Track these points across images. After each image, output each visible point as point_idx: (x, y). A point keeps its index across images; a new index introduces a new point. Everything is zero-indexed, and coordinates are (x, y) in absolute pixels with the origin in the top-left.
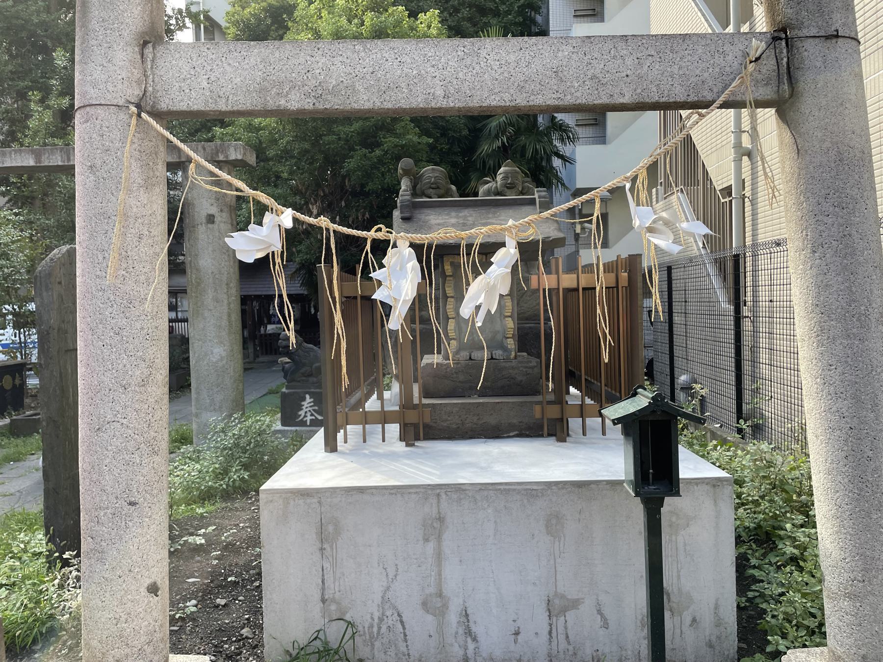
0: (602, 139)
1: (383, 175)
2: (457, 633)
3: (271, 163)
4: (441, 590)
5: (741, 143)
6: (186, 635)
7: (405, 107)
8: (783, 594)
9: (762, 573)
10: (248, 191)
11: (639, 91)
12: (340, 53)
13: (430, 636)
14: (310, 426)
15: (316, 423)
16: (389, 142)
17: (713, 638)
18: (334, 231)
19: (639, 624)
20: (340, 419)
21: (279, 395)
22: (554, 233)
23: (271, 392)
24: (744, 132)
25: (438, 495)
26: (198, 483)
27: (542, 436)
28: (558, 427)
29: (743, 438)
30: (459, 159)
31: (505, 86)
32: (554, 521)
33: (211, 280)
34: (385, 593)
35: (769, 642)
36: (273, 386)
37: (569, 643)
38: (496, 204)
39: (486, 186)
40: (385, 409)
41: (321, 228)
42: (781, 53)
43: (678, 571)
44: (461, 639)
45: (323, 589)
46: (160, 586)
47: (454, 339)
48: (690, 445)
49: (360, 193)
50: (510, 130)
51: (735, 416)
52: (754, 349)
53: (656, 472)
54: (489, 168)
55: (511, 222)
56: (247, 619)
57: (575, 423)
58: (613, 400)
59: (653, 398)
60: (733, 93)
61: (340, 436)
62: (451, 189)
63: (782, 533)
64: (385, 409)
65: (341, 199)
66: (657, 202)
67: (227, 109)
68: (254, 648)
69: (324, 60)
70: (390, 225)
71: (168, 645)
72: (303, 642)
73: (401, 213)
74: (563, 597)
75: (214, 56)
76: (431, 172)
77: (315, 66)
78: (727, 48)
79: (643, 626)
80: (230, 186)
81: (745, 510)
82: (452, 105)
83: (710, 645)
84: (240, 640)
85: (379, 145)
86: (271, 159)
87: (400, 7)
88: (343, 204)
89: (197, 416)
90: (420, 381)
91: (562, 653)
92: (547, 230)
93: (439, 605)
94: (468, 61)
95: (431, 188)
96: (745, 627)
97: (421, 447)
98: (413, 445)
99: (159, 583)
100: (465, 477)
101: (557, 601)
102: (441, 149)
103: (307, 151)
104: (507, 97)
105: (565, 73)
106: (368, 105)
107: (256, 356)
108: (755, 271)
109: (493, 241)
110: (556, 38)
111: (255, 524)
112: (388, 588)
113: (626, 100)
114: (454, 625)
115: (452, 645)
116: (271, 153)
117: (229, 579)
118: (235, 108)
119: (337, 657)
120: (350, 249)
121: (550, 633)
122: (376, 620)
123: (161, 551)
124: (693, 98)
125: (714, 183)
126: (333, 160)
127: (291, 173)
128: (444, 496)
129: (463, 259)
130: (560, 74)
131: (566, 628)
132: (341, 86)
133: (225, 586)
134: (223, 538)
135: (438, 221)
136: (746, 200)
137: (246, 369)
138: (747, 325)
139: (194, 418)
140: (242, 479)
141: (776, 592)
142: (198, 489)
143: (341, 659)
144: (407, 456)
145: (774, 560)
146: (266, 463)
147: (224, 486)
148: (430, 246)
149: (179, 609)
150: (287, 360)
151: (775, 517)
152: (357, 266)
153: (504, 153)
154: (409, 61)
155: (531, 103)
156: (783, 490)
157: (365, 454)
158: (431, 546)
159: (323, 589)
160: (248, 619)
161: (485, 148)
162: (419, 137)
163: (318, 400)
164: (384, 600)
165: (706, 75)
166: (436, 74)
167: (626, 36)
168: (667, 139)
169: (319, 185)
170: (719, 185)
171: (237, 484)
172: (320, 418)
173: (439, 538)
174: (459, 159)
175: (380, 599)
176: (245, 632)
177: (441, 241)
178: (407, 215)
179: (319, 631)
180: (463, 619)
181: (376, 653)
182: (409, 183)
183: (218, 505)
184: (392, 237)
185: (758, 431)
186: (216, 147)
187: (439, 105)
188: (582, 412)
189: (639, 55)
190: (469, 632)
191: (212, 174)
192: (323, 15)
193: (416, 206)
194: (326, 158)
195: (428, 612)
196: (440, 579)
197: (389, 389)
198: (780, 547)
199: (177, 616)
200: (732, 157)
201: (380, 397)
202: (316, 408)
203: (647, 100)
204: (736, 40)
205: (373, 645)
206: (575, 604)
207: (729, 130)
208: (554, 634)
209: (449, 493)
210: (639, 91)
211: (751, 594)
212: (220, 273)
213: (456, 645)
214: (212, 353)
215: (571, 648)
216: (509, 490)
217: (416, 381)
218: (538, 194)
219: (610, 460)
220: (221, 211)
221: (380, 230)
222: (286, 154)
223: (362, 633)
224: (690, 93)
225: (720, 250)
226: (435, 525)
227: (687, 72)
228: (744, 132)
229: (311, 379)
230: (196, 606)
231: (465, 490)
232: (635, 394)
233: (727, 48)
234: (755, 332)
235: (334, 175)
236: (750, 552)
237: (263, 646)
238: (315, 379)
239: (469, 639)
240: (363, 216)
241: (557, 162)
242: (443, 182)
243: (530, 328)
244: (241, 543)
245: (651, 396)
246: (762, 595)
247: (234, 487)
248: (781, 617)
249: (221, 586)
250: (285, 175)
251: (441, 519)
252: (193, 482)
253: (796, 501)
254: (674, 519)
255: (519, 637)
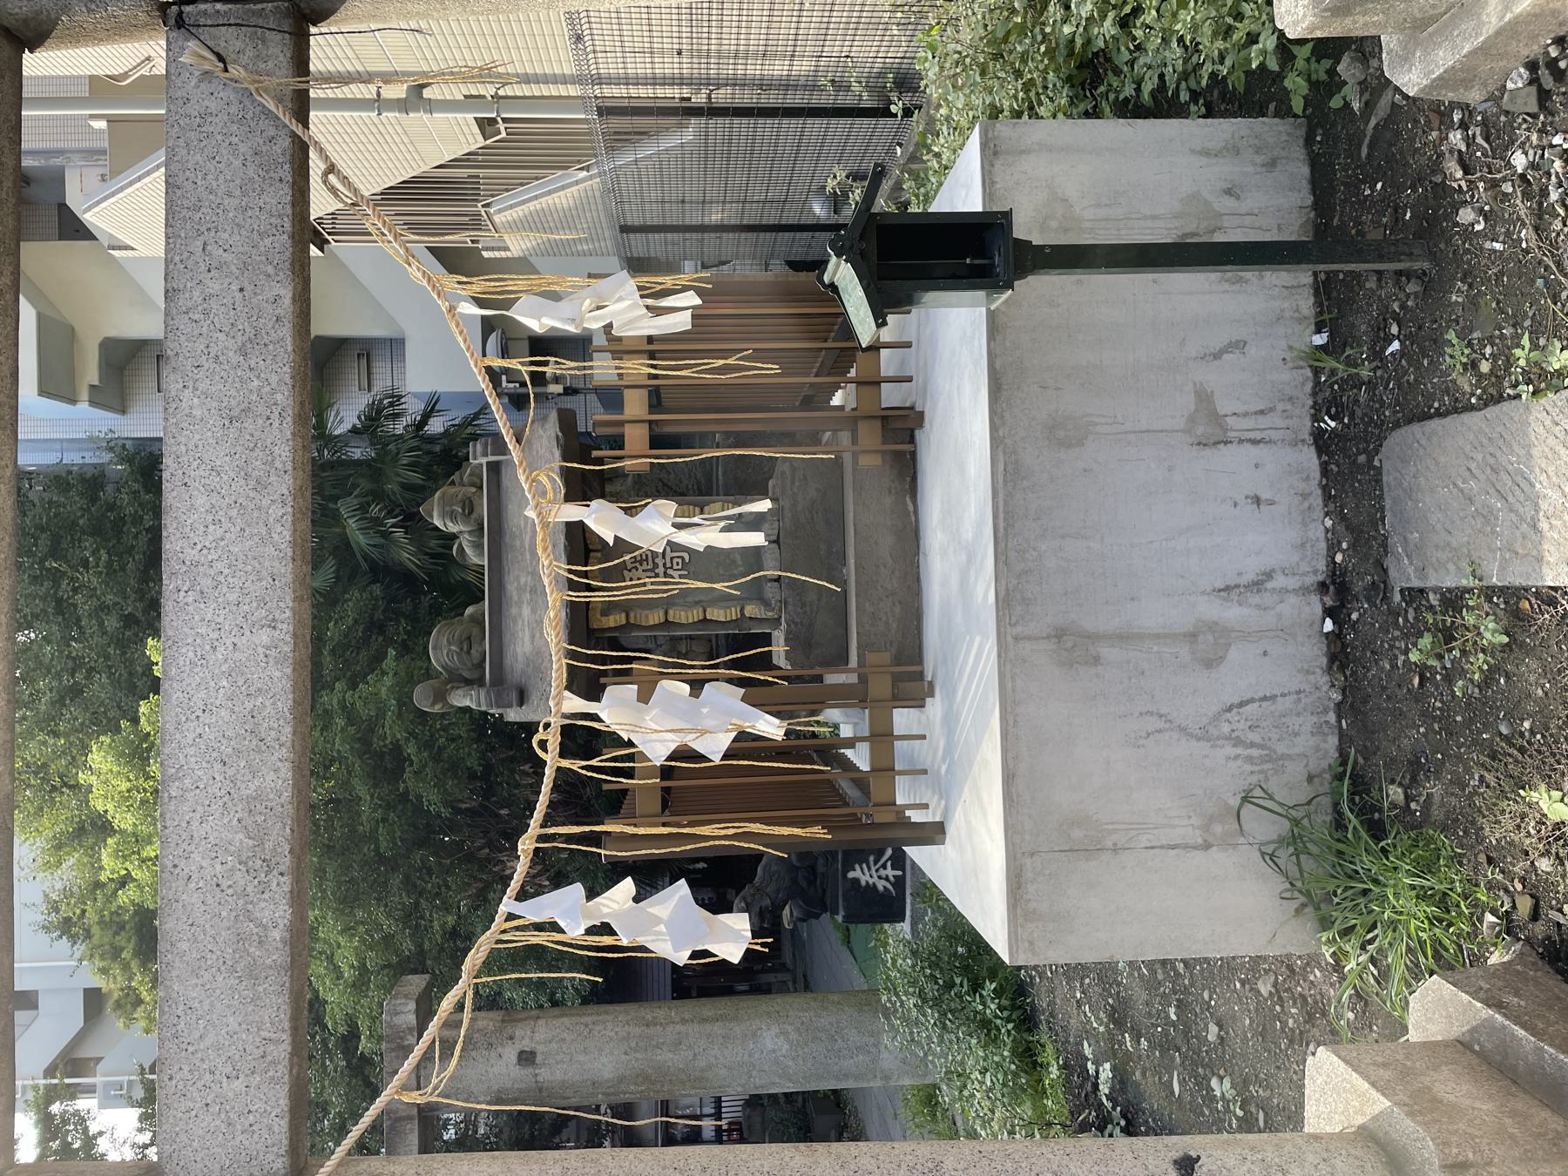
0: (395, 346)
1: (453, 740)
2: (1258, 607)
3: (427, 945)
4: (1185, 635)
5: (398, 100)
6: (1272, 1096)
7: (290, 702)
8: (1181, 40)
9: (1147, 78)
10: (463, 987)
11: (270, 269)
12: (184, 824)
13: (1265, 653)
14: (904, 870)
15: (899, 860)
16: (392, 730)
17: (1259, 159)
18: (542, 826)
19: (1236, 287)
20: (882, 817)
21: (852, 927)
22: (552, 428)
23: (847, 941)
24: (379, 94)
25: (1016, 639)
26: (1005, 1074)
27: (913, 454)
28: (898, 425)
29: (920, 108)
30: (426, 601)
31: (256, 514)
32: (1061, 434)
33: (638, 1055)
34: (1191, 735)
35: (1262, 66)
36: (837, 937)
37: (1271, 410)
38: (497, 534)
39: (468, 551)
40: (867, 734)
41: (537, 850)
42: (205, 12)
43: (1145, 218)
44: (1268, 600)
45: (1186, 847)
46: (1180, 1154)
47: (742, 610)
48: (928, 199)
49: (485, 780)
50: (375, 510)
51: (882, 121)
52: (763, 84)
53: (973, 252)
54: (443, 547)
55: (530, 513)
56: (1243, 985)
57: (891, 396)
58: (848, 332)
59: (838, 255)
60: (279, 100)
61: (916, 816)
62: (471, 616)
63: (1079, 41)
64: (867, 734)
65: (497, 816)
66: (506, 249)
67: (289, 1040)
68: (1293, 971)
69: (196, 857)
70: (530, 728)
71: (1288, 1135)
72: (1280, 884)
73: (511, 706)
74: (1192, 419)
75: (186, 1068)
76: (441, 649)
77: (208, 873)
78: (193, 109)
79: (1240, 280)
80: (452, 1024)
81: (1040, 103)
82: (288, 613)
83: (1272, 164)
84: (1280, 998)
85: (397, 748)
86: (420, 946)
87: (142, 710)
88: (504, 812)
89: (886, 1078)
90: (817, 671)
91: (1290, 422)
92: (545, 442)
93: (1210, 637)
94: (206, 583)
95: (469, 653)
96: (1240, 106)
97: (935, 668)
98: (931, 684)
99: (1177, 1155)
100: (984, 591)
101: (1200, 430)
102: (407, 633)
103: (407, 880)
104: (276, 511)
105: (233, 403)
106: (286, 771)
107: (783, 968)
108: (627, 81)
109: (562, 538)
110: (166, 419)
111: (1075, 972)
112: (1182, 729)
113: (286, 293)
114: (1245, 611)
115: (1280, 616)
116: (408, 946)
117: (1174, 1017)
118: (287, 1025)
119: (1305, 822)
120: (576, 799)
121: (1255, 442)
122: (1239, 751)
123: (1118, 1151)
124: (286, 172)
125: (473, 148)
126: (424, 831)
127: (446, 908)
128: (1019, 629)
129: (598, 598)
130: (235, 413)
131: (1246, 414)
132: (249, 821)
133: (1185, 1025)
134: (1102, 1029)
135: (527, 639)
136: (501, 93)
137: (807, 988)
138: (722, 96)
139: (892, 1083)
140: (998, 993)
141: (1179, 51)
142: (1015, 1075)
143: (1308, 816)
144: (950, 695)
145: (1126, 56)
146: (969, 951)
147: (1010, 1026)
148: (572, 655)
149: (1227, 1110)
150: (786, 911)
151: (1051, 53)
152: (606, 787)
153: (413, 521)
154: (202, 694)
155: (289, 466)
156: (1005, 40)
157: (947, 771)
158: (1108, 652)
159: (1186, 847)
160: (1243, 983)
161: (406, 554)
162: (384, 673)
163: (856, 855)
164: (1204, 736)
165: (243, 148)
166: (229, 642)
167: (167, 291)
168: (371, 229)
169: (470, 857)
170: (476, 141)
171: (1005, 1002)
172: (889, 852)
173: (1094, 637)
174: (426, 601)
175: (1201, 743)
176: (1265, 988)
177: (563, 635)
178: (514, 696)
179: (1263, 854)
180: (1234, 595)
181: (1296, 751)
182: (460, 692)
183: (1044, 1038)
184: (556, 722)
185: (907, 81)
186: (393, 1050)
187: (288, 638)
188: (871, 383)
189: (203, 268)
190: (1257, 585)
191: (427, 1057)
192: (153, 854)
193: (499, 680)
194: (421, 843)
195: (1222, 659)
196: (1166, 636)
197: (836, 726)
198: (1101, 44)
199: (1240, 1113)
200: (426, 117)
201: (851, 743)
202: (872, 858)
203: (288, 254)
204: (179, 94)
205: (1283, 757)
206: (1204, 398)
207: (376, 120)
208: (1258, 435)
209: (1014, 619)
210: (270, 269)
211: (1184, 96)
212: (627, 1038)
213: (1279, 608)
214: (774, 1051)
215: (1280, 407)
216: (1006, 512)
217: (819, 679)
218: (480, 459)
219: (952, 336)
220: (511, 1038)
221: (543, 744)
222: (411, 918)
223: (1261, 777)
224: (276, 176)
225: (592, 141)
226: (1070, 644)
227: (238, 182)
228: (379, 94)
229: (820, 869)
230: (1221, 1079)
231: (1008, 593)
232: (833, 287)
233: (193, 109)
234: (734, 82)
235: (451, 828)
236: (1112, 96)
237: (1289, 956)
238: (821, 861)
239: (1269, 585)
240: (527, 774)
241: (436, 426)
242: (459, 628)
243: (724, 473)
244: (1111, 995)
245: (834, 259)
246: (1185, 76)
247: (1013, 1008)
248: (1220, 44)
249: (1186, 1033)
250: (451, 920)
251: (1059, 634)
252: (1004, 1085)
253: (1024, 18)
254: (1054, 224)
255: (1263, 496)
